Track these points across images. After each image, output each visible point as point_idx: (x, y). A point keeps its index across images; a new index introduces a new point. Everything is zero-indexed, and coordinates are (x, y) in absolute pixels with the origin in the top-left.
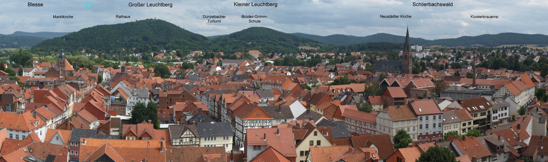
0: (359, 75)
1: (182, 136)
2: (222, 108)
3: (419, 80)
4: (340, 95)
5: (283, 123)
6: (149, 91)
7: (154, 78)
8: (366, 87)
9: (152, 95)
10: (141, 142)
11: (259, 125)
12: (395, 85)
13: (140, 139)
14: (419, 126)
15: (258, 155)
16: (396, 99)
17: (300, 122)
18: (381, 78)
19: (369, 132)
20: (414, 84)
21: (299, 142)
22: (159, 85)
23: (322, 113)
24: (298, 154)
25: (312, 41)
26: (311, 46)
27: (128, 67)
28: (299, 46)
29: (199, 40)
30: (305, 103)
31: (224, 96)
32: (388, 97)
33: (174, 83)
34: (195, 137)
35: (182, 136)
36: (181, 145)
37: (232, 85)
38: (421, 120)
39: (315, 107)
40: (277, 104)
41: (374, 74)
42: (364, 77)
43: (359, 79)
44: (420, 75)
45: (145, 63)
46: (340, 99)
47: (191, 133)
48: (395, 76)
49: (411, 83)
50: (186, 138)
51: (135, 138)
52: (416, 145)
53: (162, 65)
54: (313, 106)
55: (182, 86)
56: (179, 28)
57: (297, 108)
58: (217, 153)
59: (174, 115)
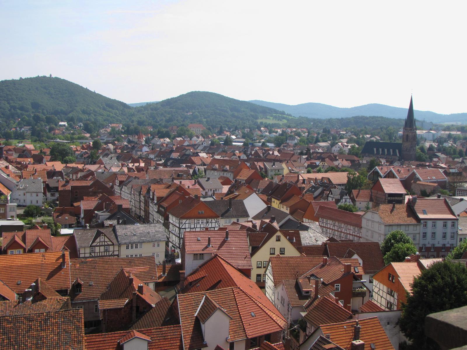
0: (340, 161)
1: (94, 244)
2: (150, 204)
3: (425, 170)
4: (313, 187)
5: (234, 223)
6: (44, 182)
7: (50, 164)
8: (348, 177)
9: (47, 188)
10: (33, 256)
11: (202, 226)
12: (390, 175)
13: (31, 251)
14: (421, 235)
15: (200, 267)
16: (391, 195)
17: (258, 223)
18: (372, 165)
19: (351, 239)
20: (418, 175)
21: (255, 250)
22: (60, 174)
23: (288, 212)
24: (254, 266)
25: (276, 111)
26: (275, 117)
27: (9, 147)
28: (257, 118)
29: (117, 109)
30: (265, 198)
31: (153, 187)
32: (380, 193)
33: (82, 170)
34: (113, 245)
35: (94, 244)
36: (93, 257)
37: (165, 171)
38: (425, 225)
39: (278, 202)
40: (226, 198)
41: (362, 160)
42: (347, 163)
43: (340, 166)
44: (427, 164)
45: (35, 141)
46: (313, 192)
47: (106, 240)
48: (391, 163)
49: (414, 174)
50: (100, 246)
51: (22, 251)
52: (416, 260)
53: (63, 144)
54: (276, 201)
55: (91, 173)
56: (87, 90)
57: (254, 204)
58: (144, 264)
59: (82, 215)
